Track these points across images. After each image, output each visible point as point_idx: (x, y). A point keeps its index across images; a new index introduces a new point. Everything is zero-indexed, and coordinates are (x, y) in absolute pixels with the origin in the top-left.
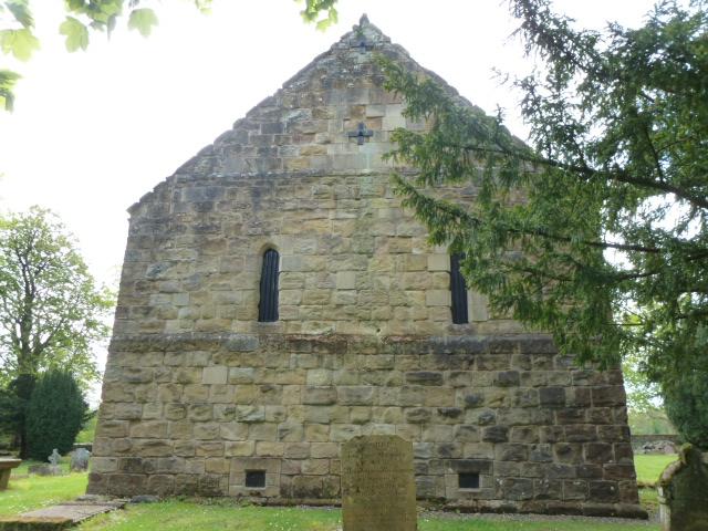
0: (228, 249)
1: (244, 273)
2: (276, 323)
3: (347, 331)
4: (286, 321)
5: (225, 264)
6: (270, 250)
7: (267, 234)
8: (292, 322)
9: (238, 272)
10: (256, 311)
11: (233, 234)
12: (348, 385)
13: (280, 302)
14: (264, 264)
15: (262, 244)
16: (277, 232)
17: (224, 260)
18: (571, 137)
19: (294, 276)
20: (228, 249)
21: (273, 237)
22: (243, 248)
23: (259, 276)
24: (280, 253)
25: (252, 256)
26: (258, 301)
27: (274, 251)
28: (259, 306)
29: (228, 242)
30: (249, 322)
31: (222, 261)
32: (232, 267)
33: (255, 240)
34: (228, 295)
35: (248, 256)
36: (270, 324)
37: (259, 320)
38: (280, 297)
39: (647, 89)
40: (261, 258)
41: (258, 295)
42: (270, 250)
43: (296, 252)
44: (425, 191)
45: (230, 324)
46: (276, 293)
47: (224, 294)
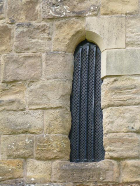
0: (15, 42)
1: (44, 81)
2: (101, 164)
3: (45, 106)
4: (118, 159)
5: (12, 67)
6: (84, 42)
7: (80, 15)
8: (130, 162)
9: (33, 81)
10: (66, 143)
11: (22, 18)
12: (117, 132)
13: (106, 128)
14: (75, 65)
15: (72, 32)
16: (96, 12)
17: (10, 60)
18: (64, 171)
19: (128, 83)
20: (15, 42)
21: (88, 19)
22: (40, 39)
23: (69, 85)
24: (103, 46)
25: (55, 53)
26: (68, 125)
27: (93, 43)
28: (70, 136)
29: (16, 32)
30: (57, 162)
31: (7, 63)
32: (23, 72)
33: (59, 27)
34: (18, 118)
35: (48, 53)
36: (90, 165)
37: (71, 160)
38: (105, 120)
39: (66, 168)
40: (70, 57)
41: (68, 117)
42: (84, 42)
43: (127, 44)
44: (73, 181)
45: (23, 167)
46: (97, 113)
47: (12, 117)
